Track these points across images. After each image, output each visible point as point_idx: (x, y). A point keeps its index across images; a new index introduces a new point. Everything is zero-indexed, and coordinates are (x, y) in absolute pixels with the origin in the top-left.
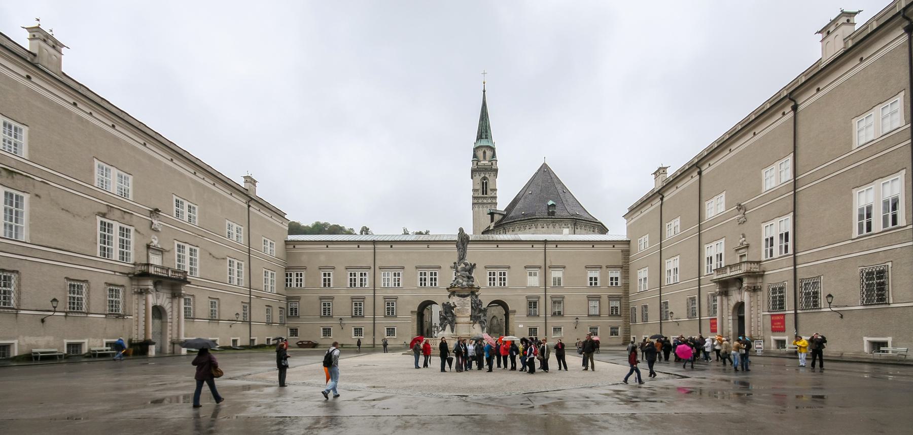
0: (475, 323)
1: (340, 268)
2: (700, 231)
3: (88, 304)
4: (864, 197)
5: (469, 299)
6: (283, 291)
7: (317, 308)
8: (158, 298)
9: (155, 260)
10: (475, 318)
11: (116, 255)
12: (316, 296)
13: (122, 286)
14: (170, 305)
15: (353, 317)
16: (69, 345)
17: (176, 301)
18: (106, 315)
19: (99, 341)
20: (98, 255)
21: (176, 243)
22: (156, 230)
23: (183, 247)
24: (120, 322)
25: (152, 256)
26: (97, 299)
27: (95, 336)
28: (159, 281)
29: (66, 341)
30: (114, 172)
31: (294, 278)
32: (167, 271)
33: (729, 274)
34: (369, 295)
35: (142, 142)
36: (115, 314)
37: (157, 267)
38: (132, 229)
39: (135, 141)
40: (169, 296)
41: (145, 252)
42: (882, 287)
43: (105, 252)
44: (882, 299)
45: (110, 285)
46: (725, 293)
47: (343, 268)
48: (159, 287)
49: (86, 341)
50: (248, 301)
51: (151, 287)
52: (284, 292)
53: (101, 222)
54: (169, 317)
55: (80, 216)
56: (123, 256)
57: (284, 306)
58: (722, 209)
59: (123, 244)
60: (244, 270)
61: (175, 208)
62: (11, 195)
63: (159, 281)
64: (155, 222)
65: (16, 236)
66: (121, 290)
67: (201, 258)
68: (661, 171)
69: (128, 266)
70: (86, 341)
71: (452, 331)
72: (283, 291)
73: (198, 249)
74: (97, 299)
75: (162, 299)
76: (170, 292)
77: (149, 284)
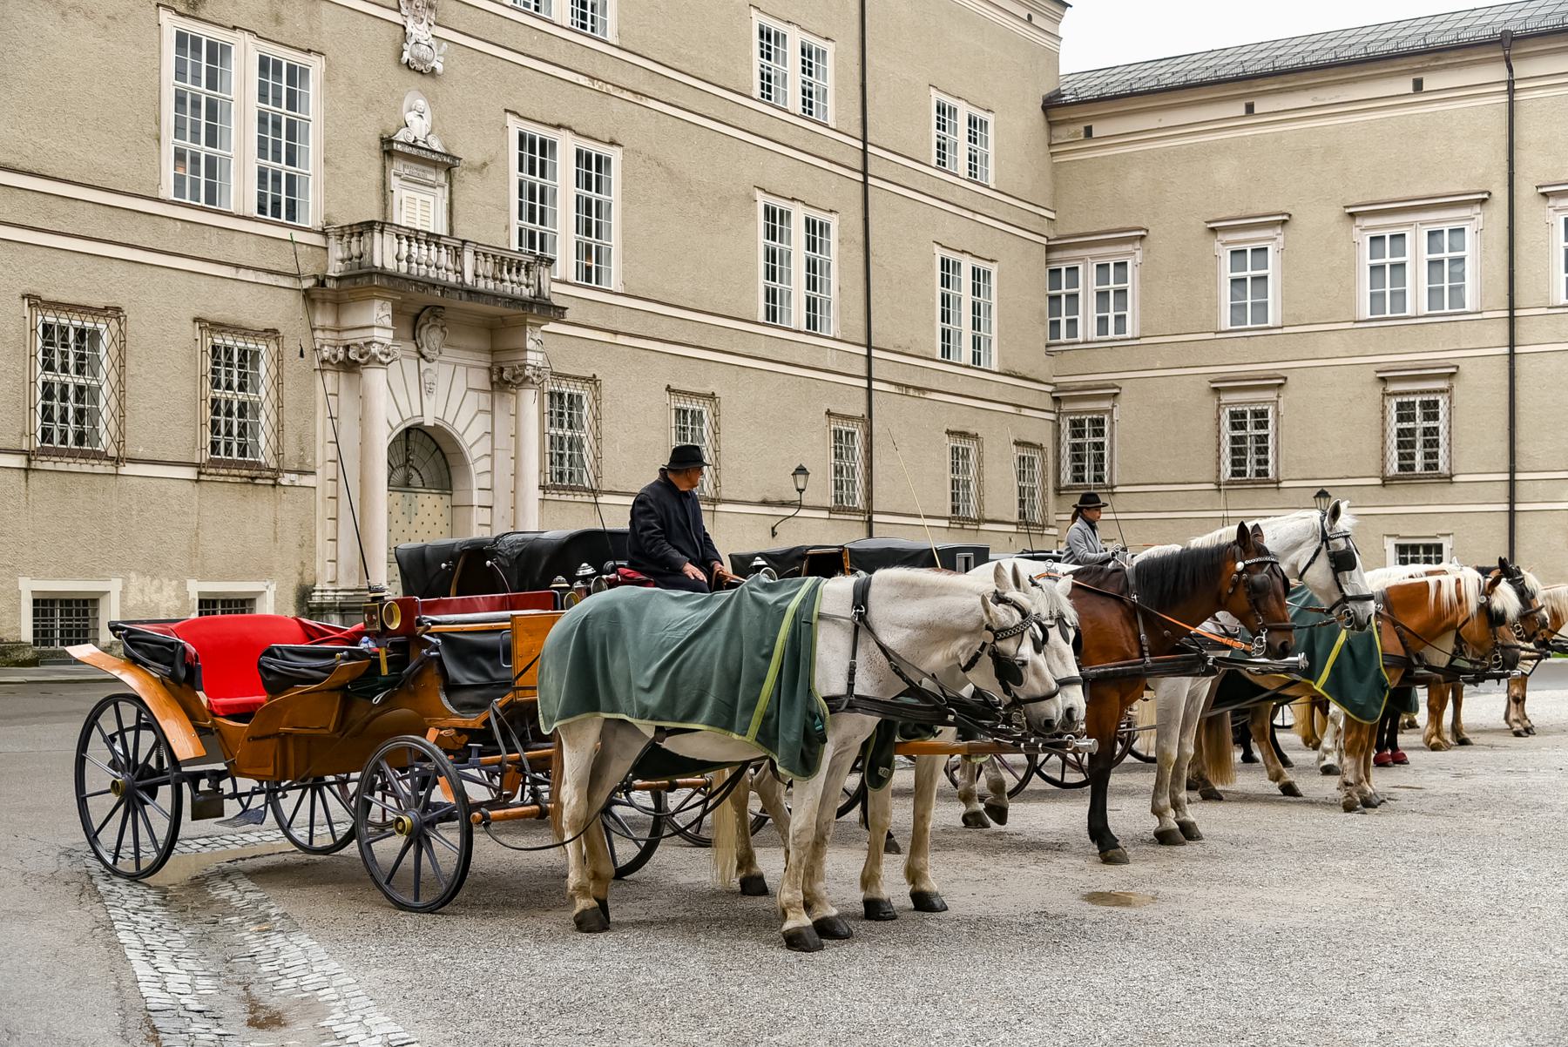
1: (1317, 218)
3: (981, 503)
6: (1033, 360)
7: (1204, 442)
8: (425, 388)
9: (420, 206)
11: (241, 191)
12: (1191, 382)
13: (272, 333)
14: (482, 423)
15: (1386, 482)
16: (43, 605)
17: (506, 403)
18: (29, 455)
19: (170, 588)
20: (168, 191)
21: (514, 126)
22: (420, 71)
23: (546, 147)
24: (259, 507)
25: (401, 193)
26: (155, 394)
27: (154, 568)
28: (426, 310)
29: (29, 587)
31: (1088, 284)
32: (457, 254)
34: (1476, 351)
35: (1024, 14)
36: (232, 454)
37: (413, 236)
38: (316, 66)
40: (480, 379)
41: (375, 175)
43: (203, 179)
45: (218, 327)
47: (1334, 213)
48: (432, 338)
49: (114, 586)
50: (861, 410)
51: (384, 336)
52: (1042, 366)
53: (181, 38)
54: (478, 481)
55: (89, 15)
56: (279, 200)
57: (1043, 436)
59: (280, 137)
60: (838, 254)
61: (757, 60)
62: (196, 42)
63: (426, 310)
64: (419, 31)
65: (211, 198)
66: (265, 350)
67: (627, 196)
69: (306, 243)
70: (114, 586)
72: (1033, 360)
73: (615, 155)
74: (155, 394)
75: (447, 391)
76: (484, 360)
77: (376, 321)
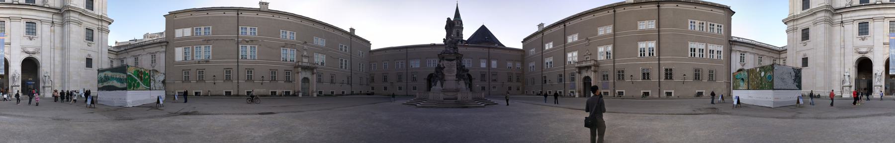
0: (459, 80)
2: (567, 48)
4: (642, 45)
5: (455, 62)
9: (305, 60)
10: (459, 77)
26: (281, 76)
30: (288, 32)
33: (584, 64)
36: (288, 80)
39: (590, 17)
42: (671, 74)
44: (671, 78)
46: (580, 73)
58: (551, 47)
68: (542, 25)
71: (442, 85)
75: (307, 74)
77: (300, 69)
